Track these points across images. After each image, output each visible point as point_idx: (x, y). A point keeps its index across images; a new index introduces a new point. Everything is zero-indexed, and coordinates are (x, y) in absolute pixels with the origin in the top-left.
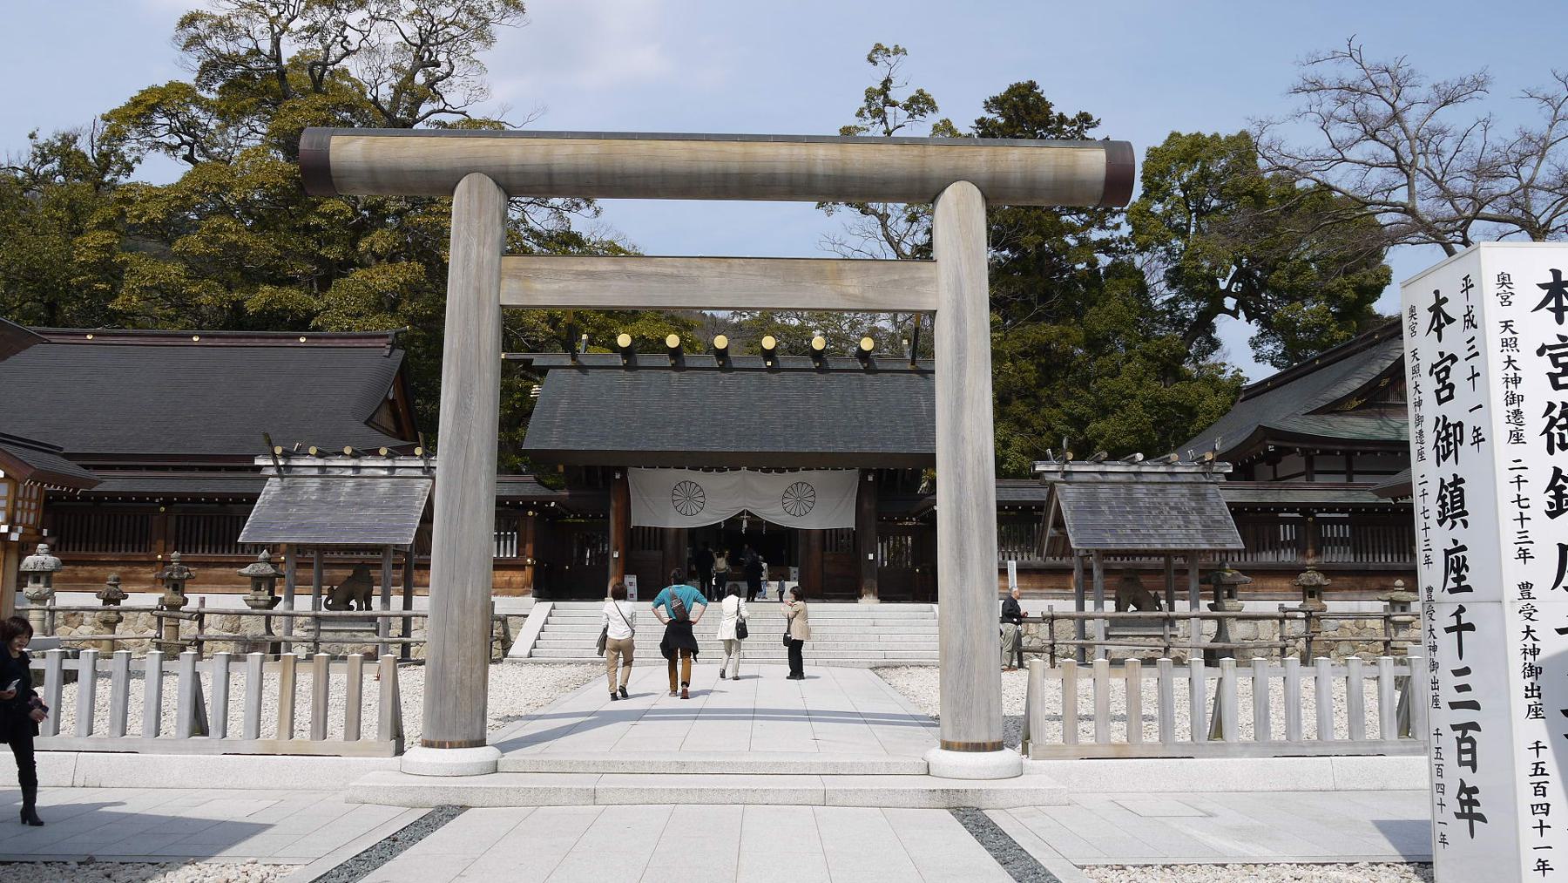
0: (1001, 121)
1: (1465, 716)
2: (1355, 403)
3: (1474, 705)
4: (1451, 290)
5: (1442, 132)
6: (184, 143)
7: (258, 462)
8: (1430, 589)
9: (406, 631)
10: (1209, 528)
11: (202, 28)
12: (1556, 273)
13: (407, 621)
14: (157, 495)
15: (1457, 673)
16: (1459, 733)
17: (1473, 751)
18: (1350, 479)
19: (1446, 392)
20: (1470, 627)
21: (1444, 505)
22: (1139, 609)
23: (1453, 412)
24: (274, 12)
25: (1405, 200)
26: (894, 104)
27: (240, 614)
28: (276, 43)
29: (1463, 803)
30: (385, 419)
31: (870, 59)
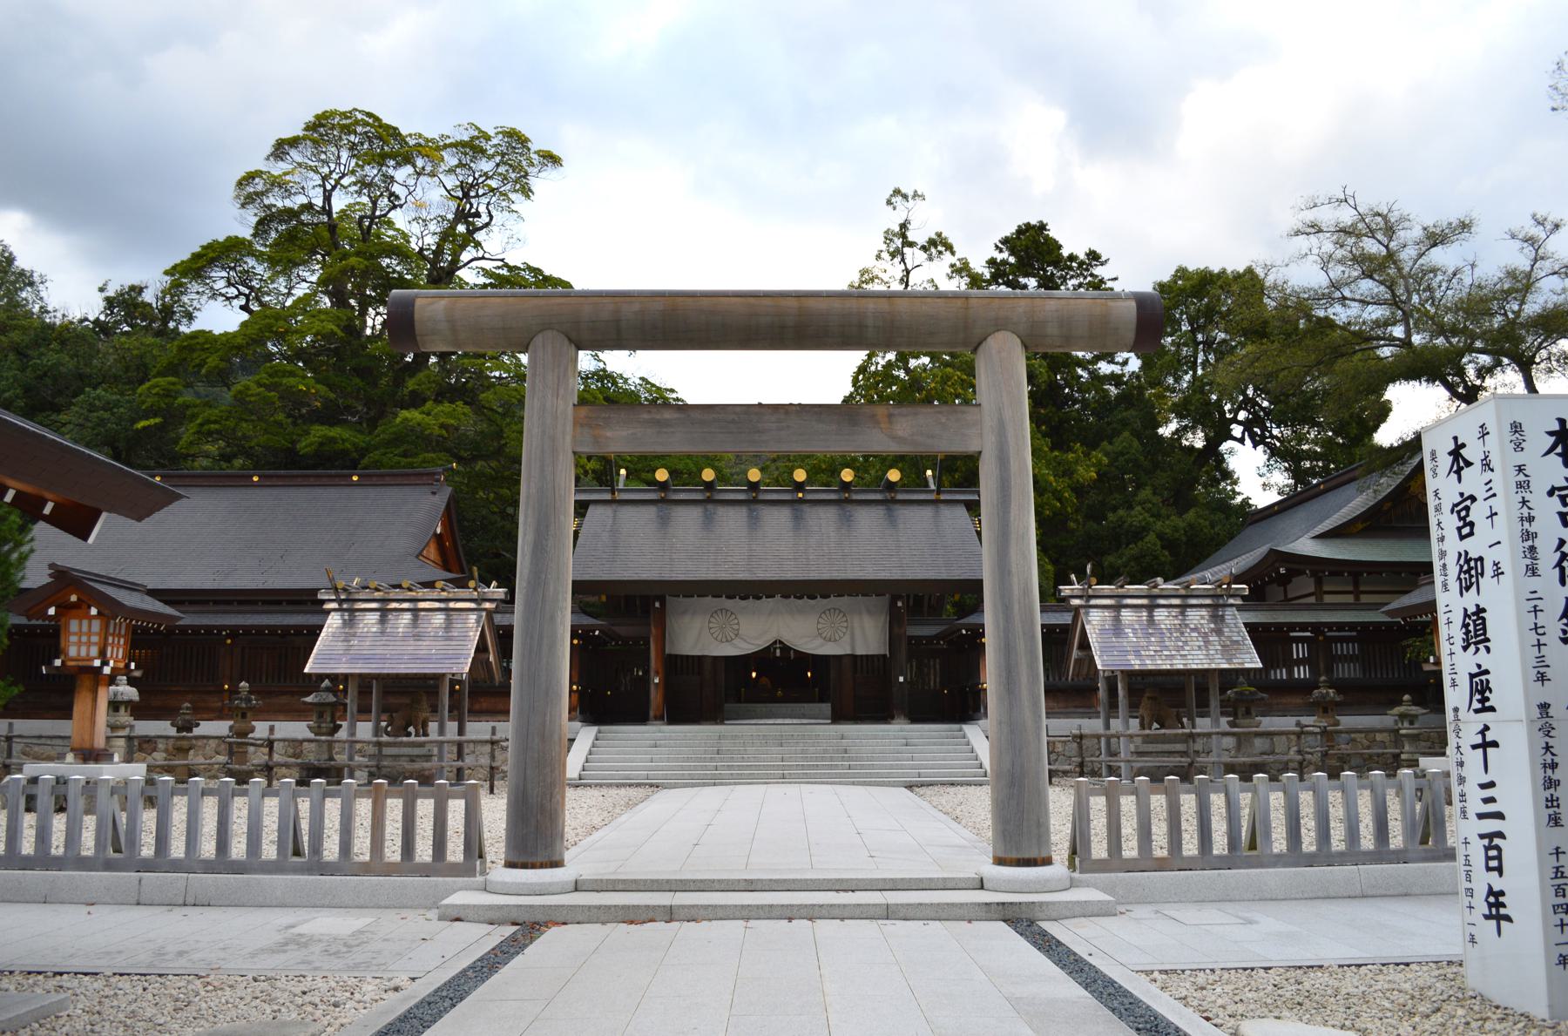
0: (1012, 260)
1: (1491, 826)
2: (1360, 526)
3: (1499, 816)
4: (1469, 437)
5: (1434, 270)
6: (240, 293)
7: (320, 597)
8: (1456, 710)
9: (460, 756)
10: (1229, 649)
11: (259, 185)
12: (1562, 421)
13: (460, 745)
14: (224, 627)
15: (1483, 786)
16: (1486, 842)
17: (1499, 858)
18: (1357, 598)
19: (1467, 529)
20: (1495, 744)
21: (1467, 633)
22: (1162, 726)
23: (1474, 547)
24: (326, 170)
25: (1402, 336)
26: (912, 245)
27: (301, 742)
28: (327, 198)
29: (1490, 905)
30: (432, 552)
31: (889, 202)
